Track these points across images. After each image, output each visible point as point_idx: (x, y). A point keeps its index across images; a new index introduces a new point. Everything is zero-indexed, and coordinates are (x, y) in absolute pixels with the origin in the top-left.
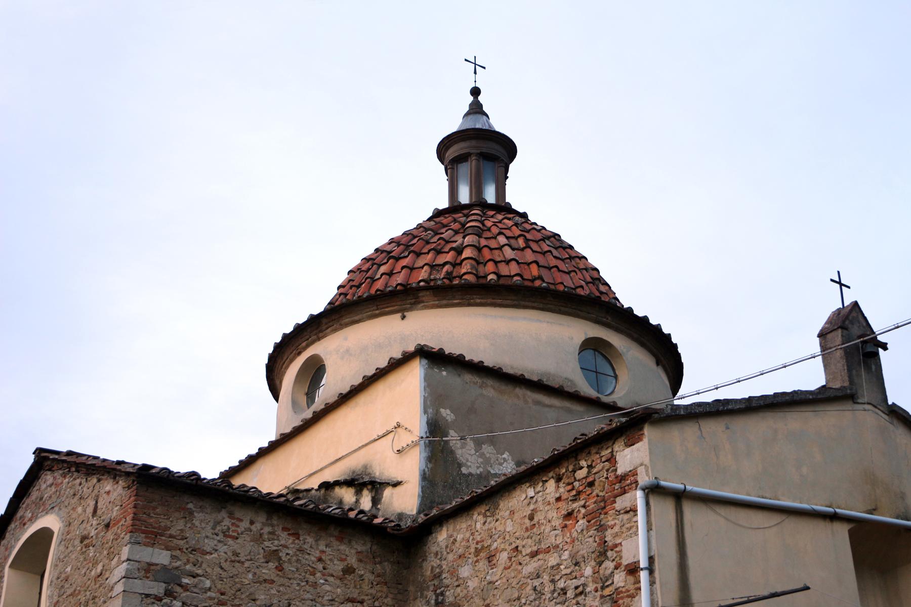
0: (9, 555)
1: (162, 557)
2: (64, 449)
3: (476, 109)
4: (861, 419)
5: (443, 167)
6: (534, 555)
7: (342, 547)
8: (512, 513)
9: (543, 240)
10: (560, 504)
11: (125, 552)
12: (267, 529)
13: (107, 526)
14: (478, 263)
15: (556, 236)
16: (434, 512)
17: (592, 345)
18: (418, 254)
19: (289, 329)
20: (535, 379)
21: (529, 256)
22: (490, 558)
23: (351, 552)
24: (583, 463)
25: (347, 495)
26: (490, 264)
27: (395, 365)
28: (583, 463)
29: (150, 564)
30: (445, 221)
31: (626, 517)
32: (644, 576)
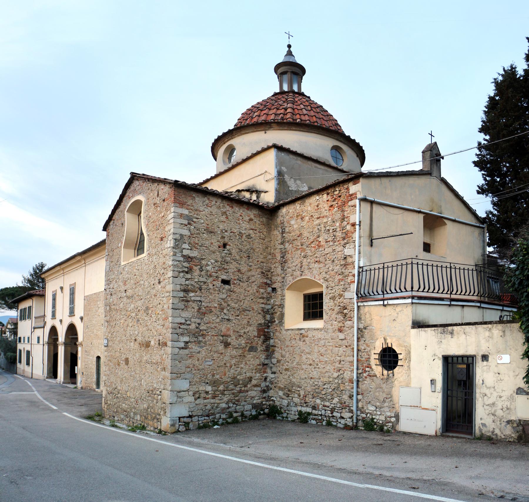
0: (126, 208)
1: (186, 212)
2: (141, 173)
3: (290, 53)
4: (433, 181)
5: (276, 76)
6: (318, 218)
7: (248, 212)
8: (310, 204)
9: (317, 107)
10: (328, 202)
11: (172, 209)
12: (222, 205)
13: (164, 200)
14: (293, 114)
15: (321, 106)
16: (281, 202)
17: (336, 148)
18: (270, 109)
19: (220, 134)
20: (315, 159)
21: (312, 113)
22: (302, 219)
23: (252, 213)
24: (337, 189)
25: (247, 195)
26: (298, 115)
27: (264, 150)
28: (337, 189)
29: (182, 214)
30: (279, 97)
31: (352, 208)
32: (357, 227)
